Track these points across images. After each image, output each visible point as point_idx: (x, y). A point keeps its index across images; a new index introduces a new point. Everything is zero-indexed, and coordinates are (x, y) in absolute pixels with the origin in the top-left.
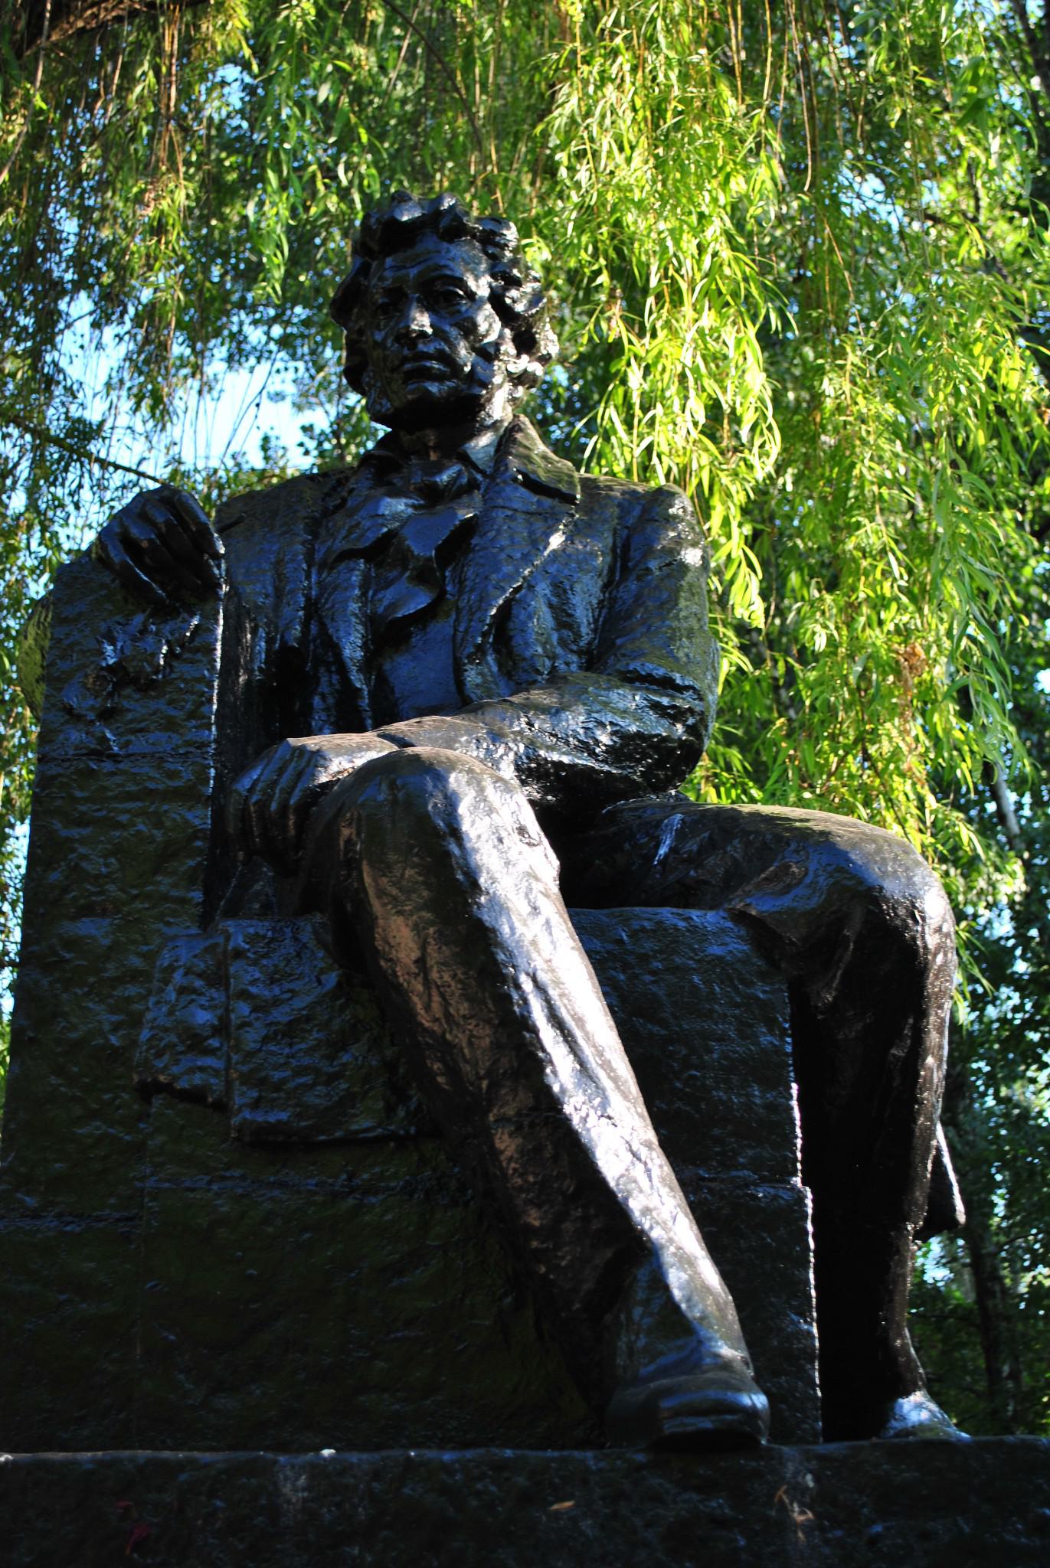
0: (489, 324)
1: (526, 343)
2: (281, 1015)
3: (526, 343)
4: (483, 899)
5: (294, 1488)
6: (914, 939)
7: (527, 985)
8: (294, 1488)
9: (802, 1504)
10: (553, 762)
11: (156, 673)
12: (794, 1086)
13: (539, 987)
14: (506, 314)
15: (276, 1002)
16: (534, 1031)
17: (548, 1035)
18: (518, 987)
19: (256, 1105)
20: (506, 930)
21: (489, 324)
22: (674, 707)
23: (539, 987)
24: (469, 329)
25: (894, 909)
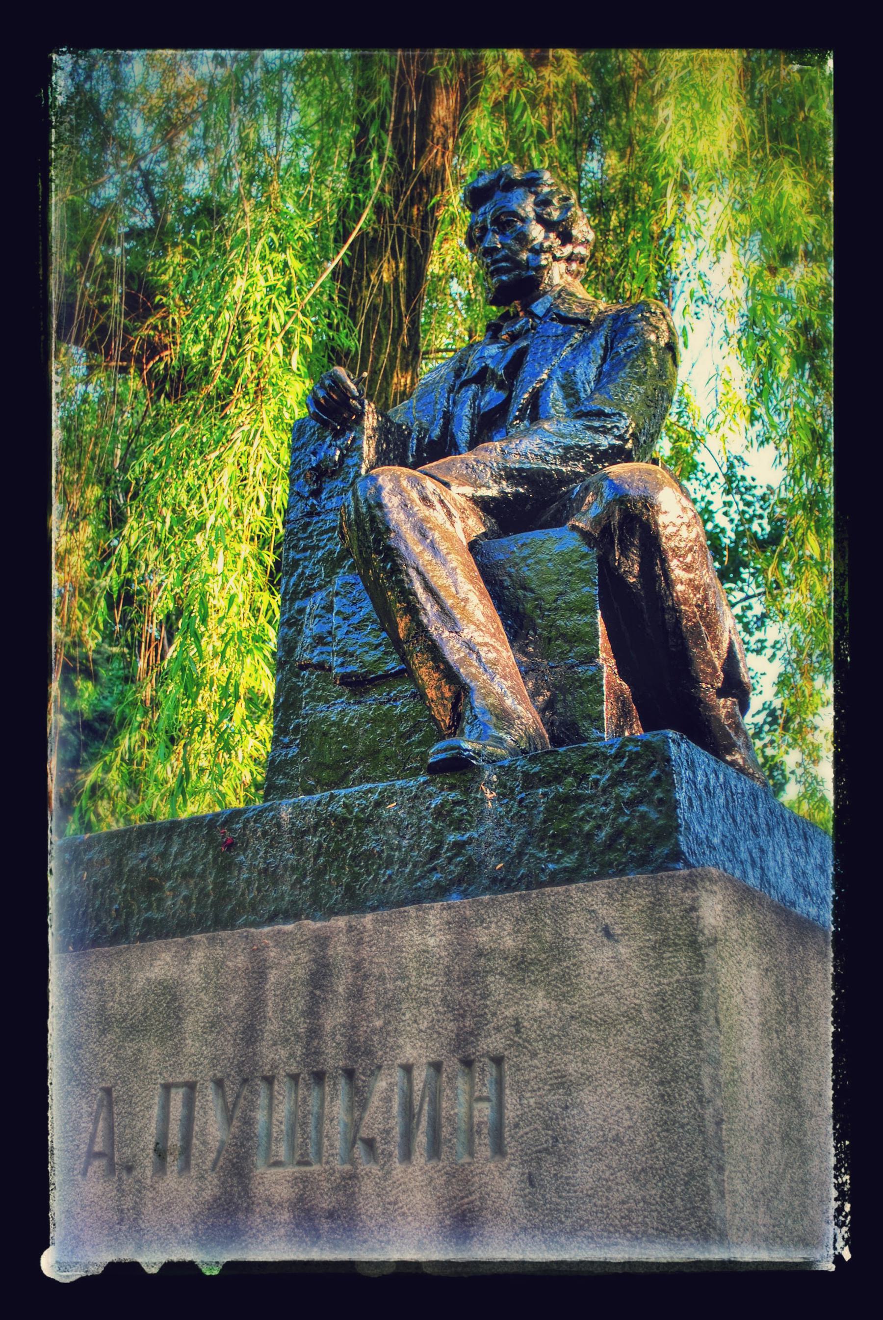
0: (537, 232)
1: (566, 238)
2: (355, 620)
3: (566, 238)
4: (392, 535)
5: (286, 814)
6: (647, 520)
7: (413, 574)
8: (286, 814)
9: (491, 790)
10: (516, 469)
11: (335, 465)
12: (599, 612)
13: (419, 573)
14: (549, 225)
15: (354, 614)
16: (415, 594)
17: (422, 595)
18: (408, 575)
19: (342, 665)
20: (403, 548)
21: (537, 232)
22: (603, 426)
23: (419, 573)
24: (523, 238)
25: (635, 505)
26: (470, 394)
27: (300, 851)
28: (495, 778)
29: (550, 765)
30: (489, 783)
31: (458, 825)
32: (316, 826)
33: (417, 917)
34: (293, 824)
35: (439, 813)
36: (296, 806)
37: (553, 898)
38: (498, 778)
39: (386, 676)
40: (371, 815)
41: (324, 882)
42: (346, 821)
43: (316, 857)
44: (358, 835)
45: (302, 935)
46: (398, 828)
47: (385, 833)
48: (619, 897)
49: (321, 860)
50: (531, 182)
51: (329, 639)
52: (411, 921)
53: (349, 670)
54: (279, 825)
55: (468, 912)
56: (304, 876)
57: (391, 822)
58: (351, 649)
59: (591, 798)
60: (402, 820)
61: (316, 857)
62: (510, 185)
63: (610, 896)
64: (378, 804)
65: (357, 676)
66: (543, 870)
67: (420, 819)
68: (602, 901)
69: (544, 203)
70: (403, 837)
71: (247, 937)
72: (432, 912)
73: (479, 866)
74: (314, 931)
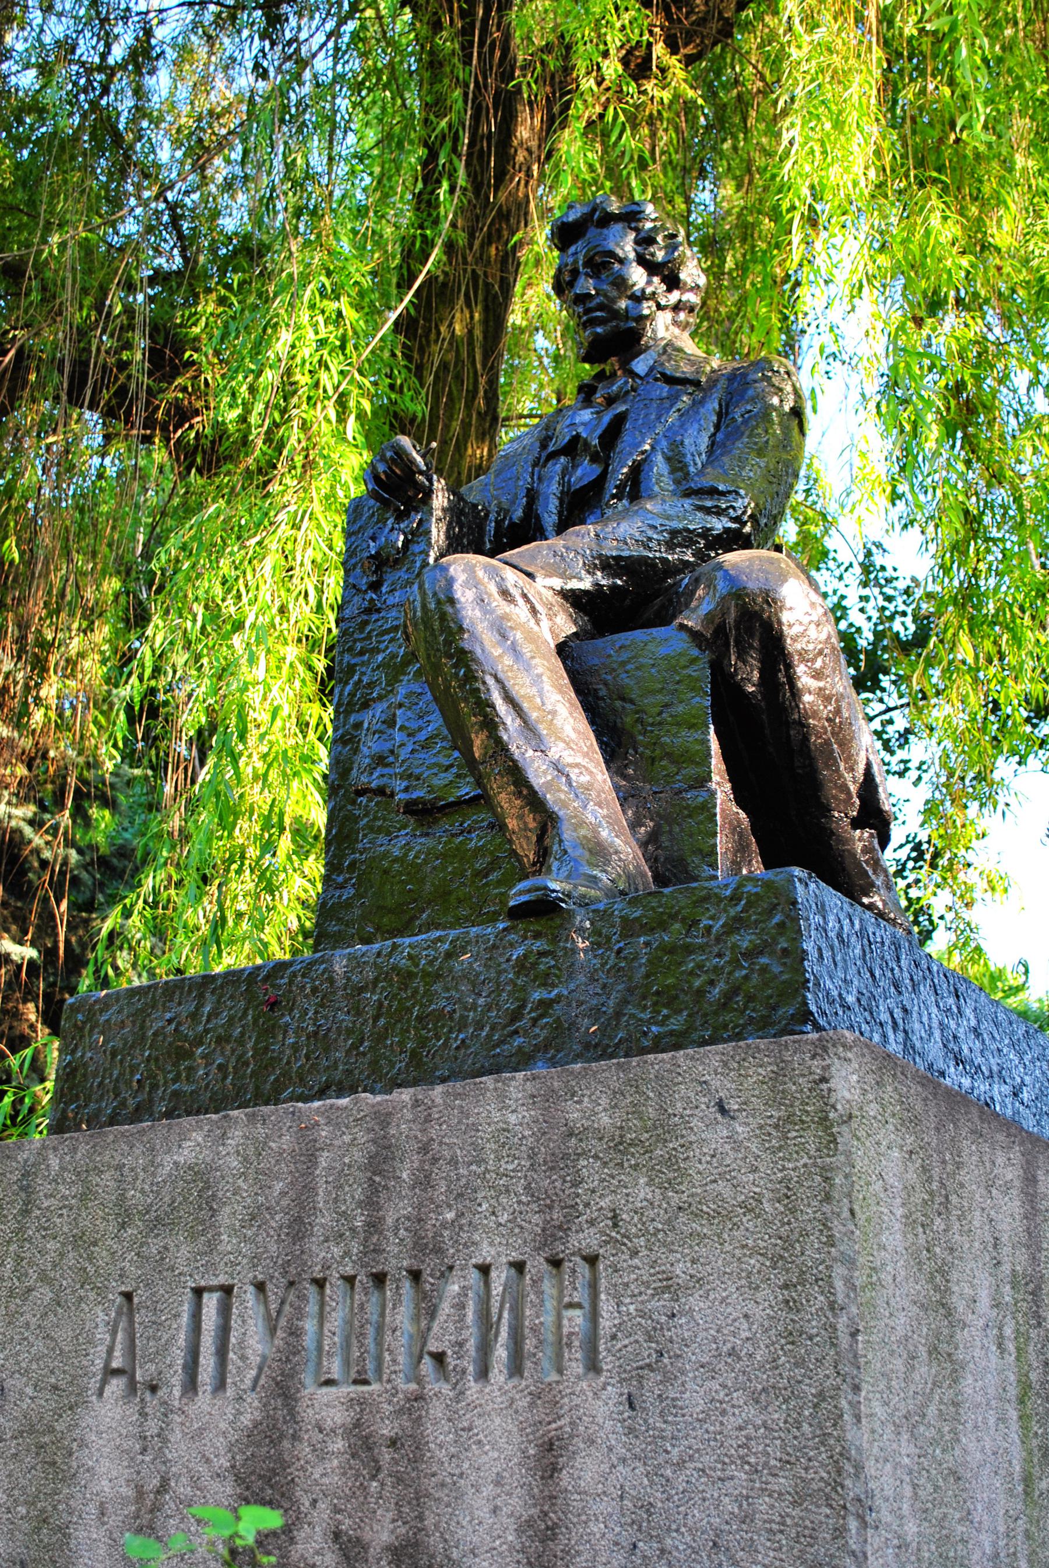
0: (638, 276)
2: (422, 736)
7: (490, 681)
15: (420, 729)
27: (357, 1011)
28: (588, 924)
30: (581, 930)
31: (545, 980)
32: (376, 981)
34: (349, 979)
35: (522, 966)
36: (351, 957)
39: (459, 803)
40: (440, 968)
42: (411, 975)
43: (376, 1019)
49: (382, 1022)
51: (391, 759)
54: (331, 981)
59: (702, 948)
60: (478, 975)
62: (607, 219)
63: (725, 1064)
64: (449, 955)
65: (424, 803)
66: (645, 1034)
67: (499, 973)
69: (646, 241)
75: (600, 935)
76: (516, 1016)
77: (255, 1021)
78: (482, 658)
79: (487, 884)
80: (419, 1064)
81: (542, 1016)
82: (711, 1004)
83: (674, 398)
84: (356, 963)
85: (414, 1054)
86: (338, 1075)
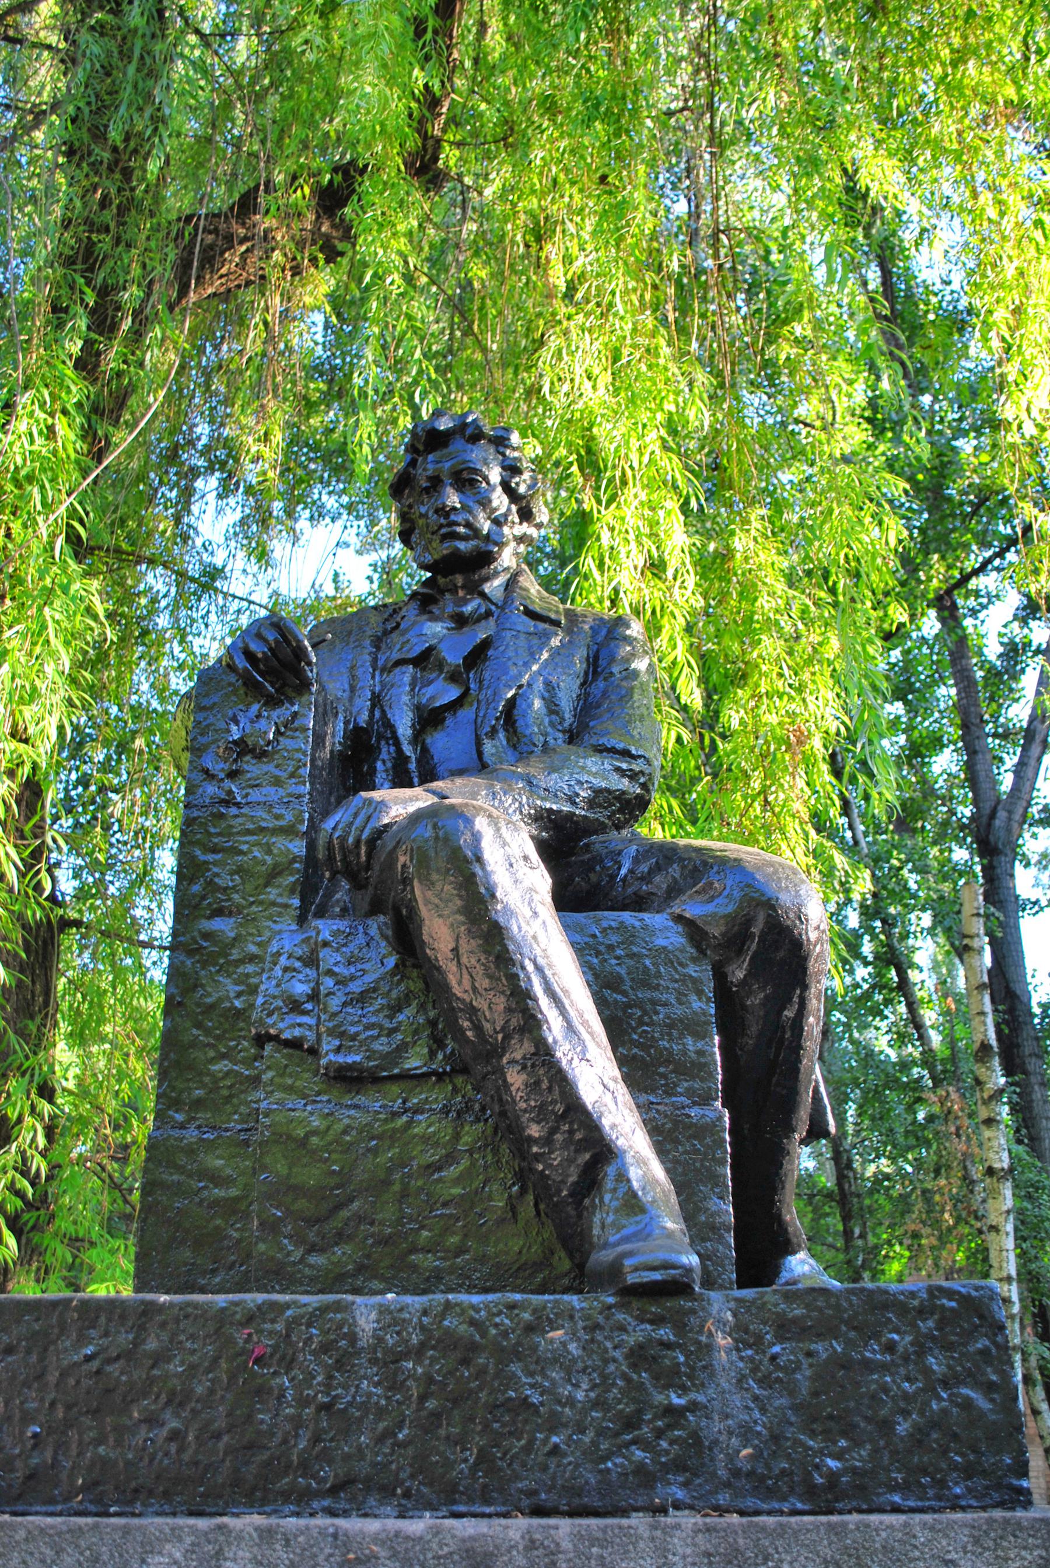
0: (500, 500)
2: (356, 987)
7: (530, 967)
13: (538, 969)
15: (353, 978)
18: (523, 968)
26: (407, 679)
27: (394, 1384)
28: (729, 1316)
29: (820, 1310)
30: (720, 1322)
31: (670, 1379)
32: (423, 1346)
33: (653, 1539)
34: (380, 1340)
35: (639, 1356)
36: (383, 1310)
37: (884, 1534)
38: (735, 1315)
39: (405, 1076)
40: (519, 1343)
41: (438, 1439)
42: (474, 1348)
43: (423, 1398)
44: (497, 1375)
45: (441, 1545)
46: (569, 1372)
47: (545, 1376)
48: (991, 1544)
49: (431, 1404)
50: (500, 442)
51: (309, 1006)
52: (641, 1545)
53: (349, 1060)
54: (353, 1338)
55: (741, 1541)
56: (400, 1426)
57: (555, 1360)
58: (353, 1030)
59: (884, 1367)
60: (574, 1361)
61: (423, 1398)
62: (476, 436)
63: (977, 1541)
64: (530, 1328)
65: (361, 1071)
66: (817, 1467)
67: (606, 1361)
68: (964, 1548)
69: (512, 469)
70: (576, 1386)
71: (335, 1536)
72: (678, 1533)
73: (710, 1449)
74: (464, 1541)
75: (746, 1331)
76: (631, 1423)
77: (233, 1377)
78: (519, 938)
79: (440, 1180)
80: (492, 1470)
81: (670, 1427)
82: (902, 1438)
83: (546, 636)
84: (391, 1319)
85: (483, 1457)
86: (363, 1469)
